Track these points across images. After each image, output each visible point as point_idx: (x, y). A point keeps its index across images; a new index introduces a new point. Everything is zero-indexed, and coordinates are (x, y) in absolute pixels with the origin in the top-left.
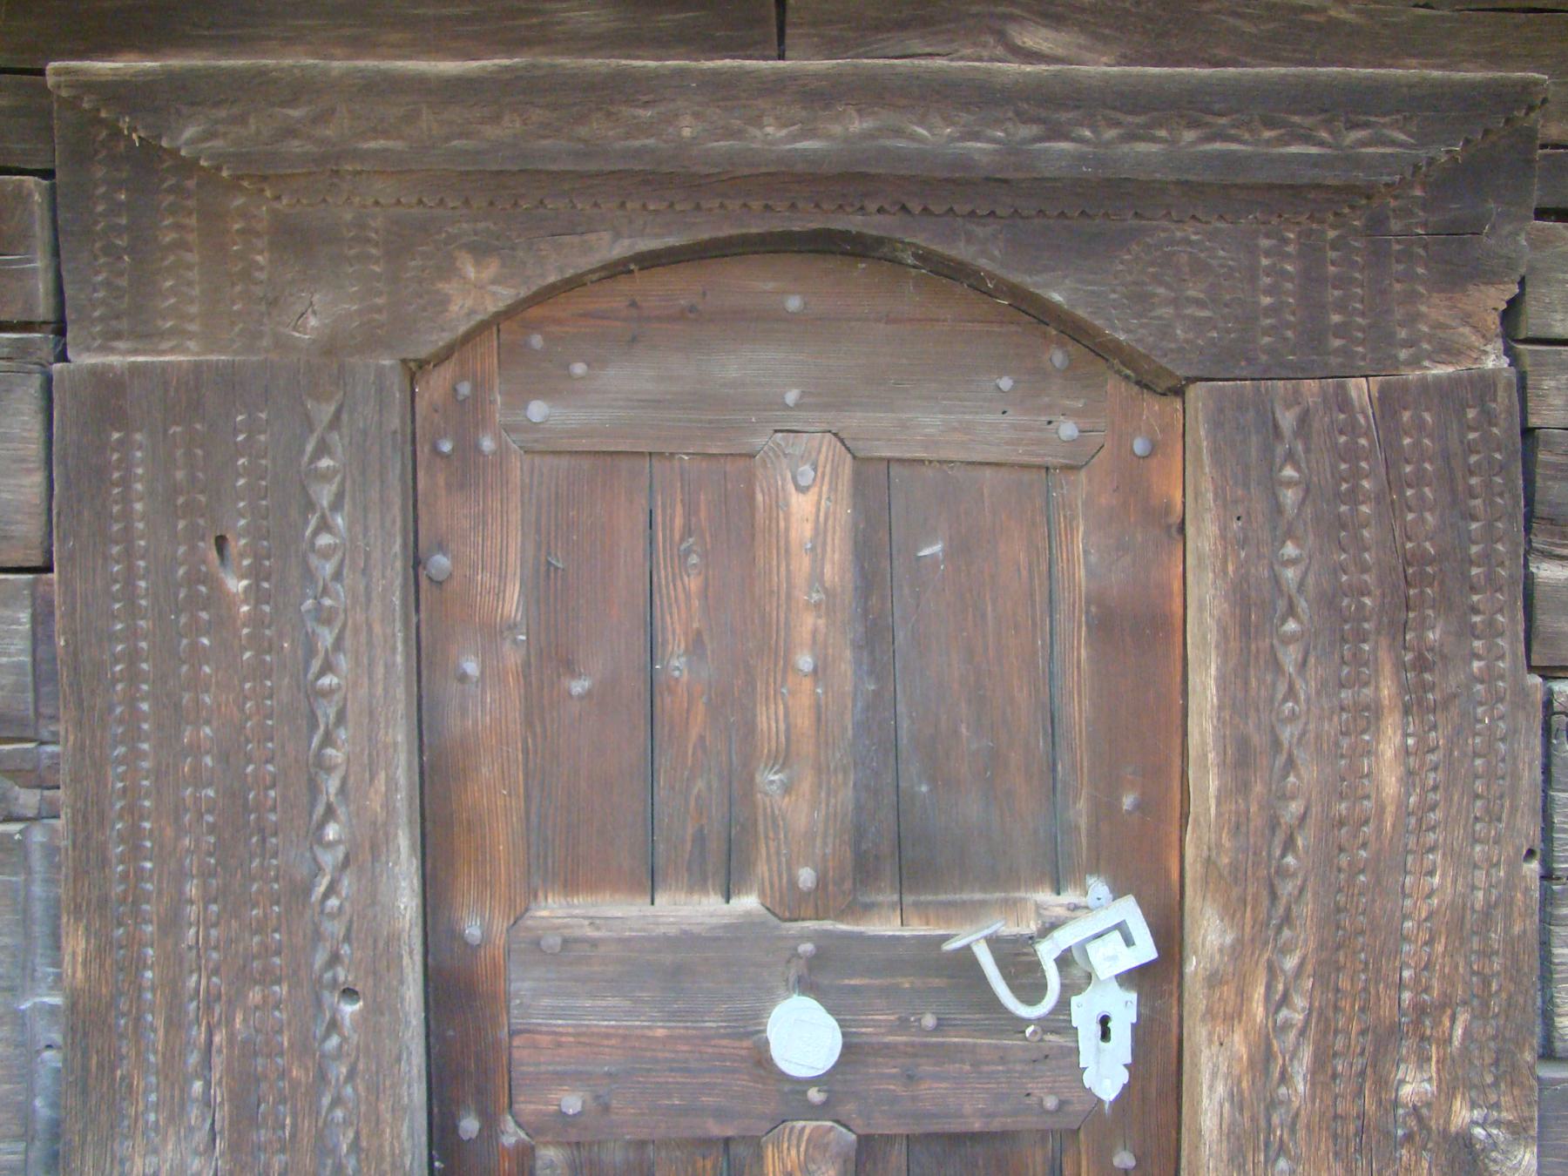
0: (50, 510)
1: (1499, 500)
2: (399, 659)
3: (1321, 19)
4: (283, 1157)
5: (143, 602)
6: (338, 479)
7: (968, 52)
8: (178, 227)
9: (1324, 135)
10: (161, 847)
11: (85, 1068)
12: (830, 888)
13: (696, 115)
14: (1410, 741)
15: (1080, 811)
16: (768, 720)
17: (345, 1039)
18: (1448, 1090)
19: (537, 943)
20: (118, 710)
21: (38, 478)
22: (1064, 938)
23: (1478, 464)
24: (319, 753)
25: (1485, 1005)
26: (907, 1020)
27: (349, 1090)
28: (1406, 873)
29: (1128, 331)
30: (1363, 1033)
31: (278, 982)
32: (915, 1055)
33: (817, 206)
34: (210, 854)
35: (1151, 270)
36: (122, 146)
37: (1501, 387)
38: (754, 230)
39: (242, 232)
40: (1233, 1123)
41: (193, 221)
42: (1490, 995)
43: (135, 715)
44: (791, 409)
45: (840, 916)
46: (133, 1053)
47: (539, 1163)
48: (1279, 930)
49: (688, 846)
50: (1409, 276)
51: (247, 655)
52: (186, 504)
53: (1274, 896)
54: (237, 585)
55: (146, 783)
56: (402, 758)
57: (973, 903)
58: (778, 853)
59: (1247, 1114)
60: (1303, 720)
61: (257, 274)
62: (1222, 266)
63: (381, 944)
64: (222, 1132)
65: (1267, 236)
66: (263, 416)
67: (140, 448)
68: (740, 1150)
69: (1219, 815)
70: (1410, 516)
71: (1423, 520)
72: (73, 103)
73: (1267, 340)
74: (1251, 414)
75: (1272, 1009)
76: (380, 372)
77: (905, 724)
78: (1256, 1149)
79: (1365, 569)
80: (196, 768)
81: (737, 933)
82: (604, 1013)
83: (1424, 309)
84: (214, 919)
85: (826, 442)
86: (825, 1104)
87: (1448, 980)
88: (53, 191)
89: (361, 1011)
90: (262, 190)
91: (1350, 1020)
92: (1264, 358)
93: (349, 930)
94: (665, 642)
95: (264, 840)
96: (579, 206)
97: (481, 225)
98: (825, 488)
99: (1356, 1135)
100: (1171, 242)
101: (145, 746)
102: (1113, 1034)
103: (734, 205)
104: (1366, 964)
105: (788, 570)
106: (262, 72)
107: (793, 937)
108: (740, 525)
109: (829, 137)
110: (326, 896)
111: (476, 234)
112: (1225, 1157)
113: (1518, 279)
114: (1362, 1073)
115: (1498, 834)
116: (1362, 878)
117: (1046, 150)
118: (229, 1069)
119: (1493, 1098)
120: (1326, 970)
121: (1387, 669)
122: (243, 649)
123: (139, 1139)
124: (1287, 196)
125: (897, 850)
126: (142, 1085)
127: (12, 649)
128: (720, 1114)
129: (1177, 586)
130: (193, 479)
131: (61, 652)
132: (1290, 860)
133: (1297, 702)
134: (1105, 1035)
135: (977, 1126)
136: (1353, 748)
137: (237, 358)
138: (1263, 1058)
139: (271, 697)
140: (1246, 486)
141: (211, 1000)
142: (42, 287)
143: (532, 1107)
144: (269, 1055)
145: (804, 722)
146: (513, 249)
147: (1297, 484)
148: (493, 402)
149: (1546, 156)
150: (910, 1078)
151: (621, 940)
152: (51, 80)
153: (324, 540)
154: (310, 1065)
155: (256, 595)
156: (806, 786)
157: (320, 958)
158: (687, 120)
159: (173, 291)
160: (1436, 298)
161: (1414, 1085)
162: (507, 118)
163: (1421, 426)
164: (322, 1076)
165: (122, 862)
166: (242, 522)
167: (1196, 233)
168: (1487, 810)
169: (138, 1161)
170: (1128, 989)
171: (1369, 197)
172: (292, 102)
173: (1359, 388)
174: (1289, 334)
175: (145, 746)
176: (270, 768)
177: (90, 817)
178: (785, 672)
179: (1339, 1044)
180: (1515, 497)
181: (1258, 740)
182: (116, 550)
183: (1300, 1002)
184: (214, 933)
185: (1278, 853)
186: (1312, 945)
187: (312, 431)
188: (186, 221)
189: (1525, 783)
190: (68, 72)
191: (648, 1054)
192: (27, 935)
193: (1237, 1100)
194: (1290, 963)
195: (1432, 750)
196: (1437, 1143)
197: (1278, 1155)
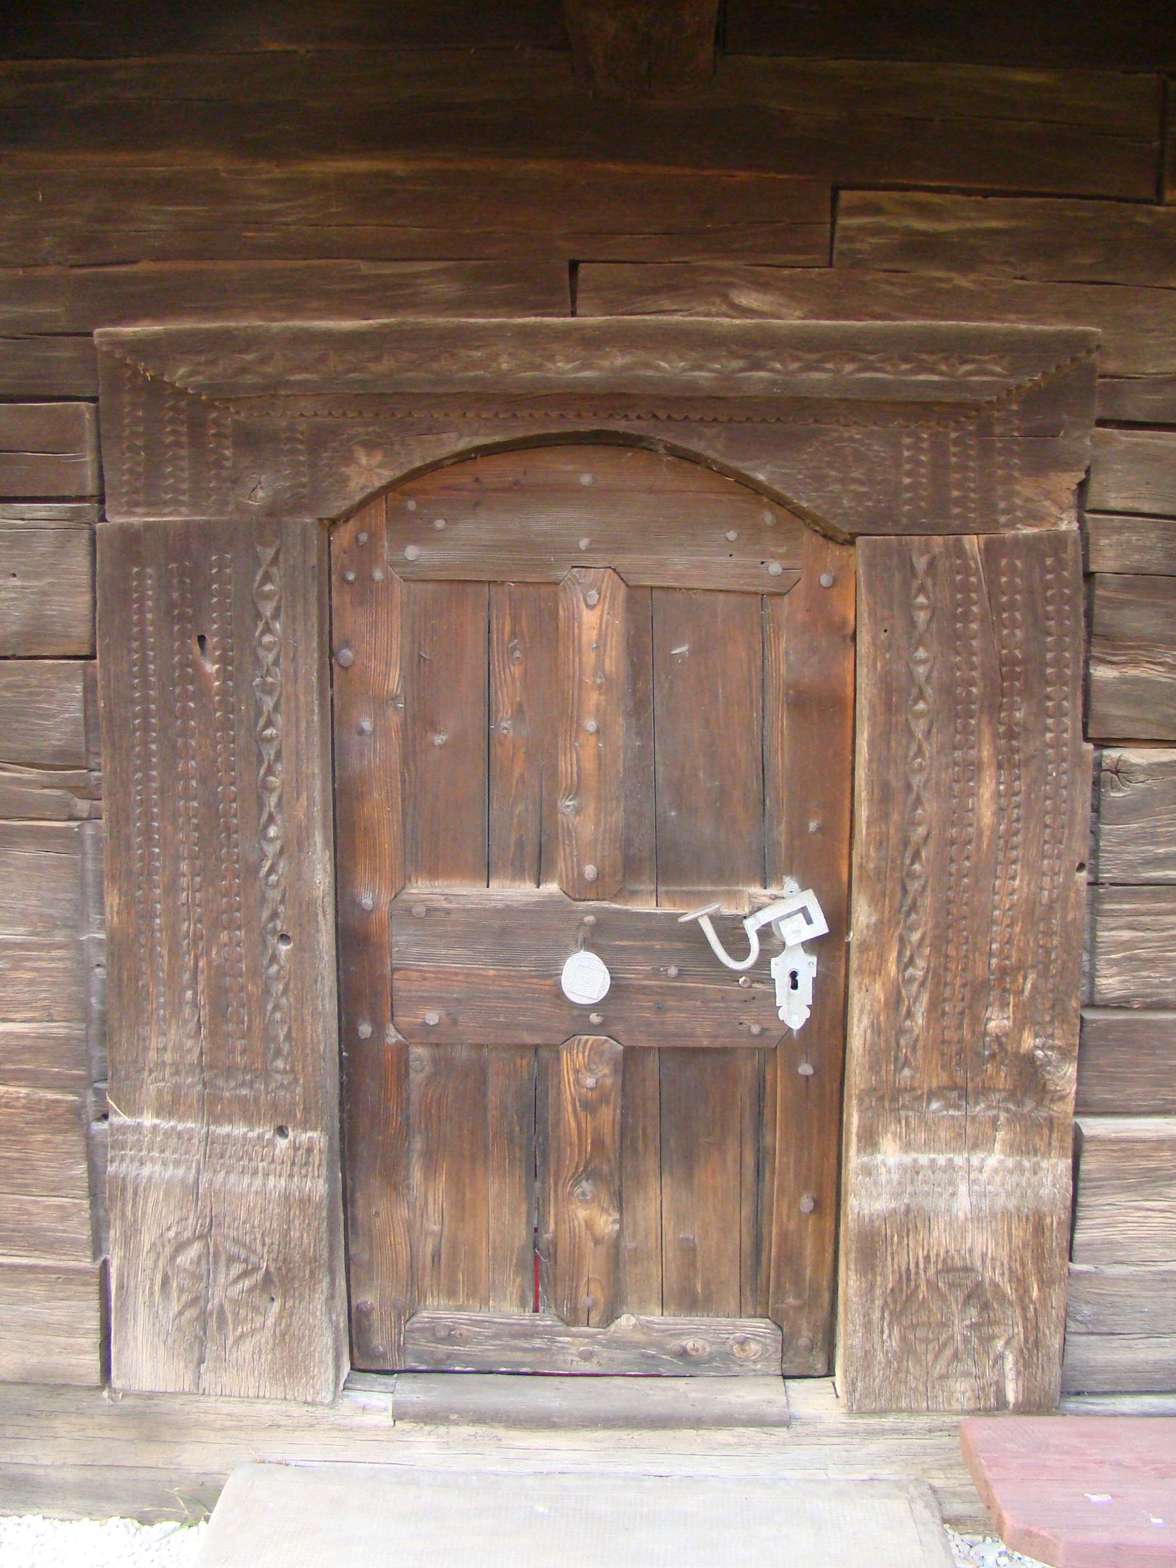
0: (94, 618)
1: (1067, 622)
2: (316, 718)
4: (243, 1042)
5: (153, 679)
6: (276, 598)
7: (702, 309)
8: (174, 432)
9: (944, 368)
10: (165, 839)
11: (120, 979)
12: (607, 879)
13: (510, 355)
14: (1002, 787)
15: (781, 832)
16: (566, 765)
17: (281, 967)
20: (137, 749)
21: (87, 598)
22: (764, 917)
23: (1053, 596)
24: (264, 780)
25: (1047, 968)
26: (658, 970)
27: (284, 1000)
28: (997, 877)
29: (809, 500)
30: (964, 985)
31: (239, 928)
33: (595, 414)
34: (195, 844)
35: (827, 459)
36: (140, 381)
38: (553, 431)
39: (214, 435)
40: (872, 1044)
41: (184, 429)
42: (1051, 962)
43: (148, 754)
44: (582, 552)
45: (614, 897)
46: (149, 971)
47: (412, 1057)
48: (908, 914)
49: (512, 849)
50: (1005, 465)
51: (218, 714)
52: (179, 614)
53: (905, 891)
54: (211, 668)
56: (318, 783)
57: (706, 892)
58: (571, 853)
59: (883, 1038)
60: (927, 771)
62: (876, 457)
65: (908, 436)
66: (228, 556)
67: (150, 577)
68: (543, 1053)
69: (868, 834)
70: (1005, 632)
71: (1013, 635)
72: (109, 355)
73: (907, 508)
74: (895, 559)
75: (902, 967)
77: (661, 769)
78: (888, 1062)
79: (973, 667)
82: (454, 959)
83: (1018, 488)
85: (607, 576)
86: (601, 1024)
88: (97, 411)
89: (292, 950)
90: (228, 408)
91: (955, 977)
92: (904, 520)
93: (284, 896)
94: (497, 711)
95: (229, 836)
96: (435, 416)
97: (371, 429)
99: (957, 1054)
101: (154, 773)
102: (788, 975)
103: (538, 414)
104: (967, 938)
108: (548, 631)
109: (600, 369)
110: (269, 873)
112: (867, 1066)
113: (1085, 468)
114: (962, 1013)
116: (966, 880)
117: (749, 378)
119: (1049, 1031)
121: (987, 736)
122: (216, 710)
124: (921, 409)
125: (654, 856)
128: (531, 1029)
129: (850, 678)
130: (183, 597)
131: (101, 712)
132: (917, 867)
133: (924, 758)
134: (795, 986)
135: (706, 1043)
136: (962, 791)
137: (213, 518)
138: (895, 1001)
139: (233, 742)
140: (891, 609)
141: (197, 938)
142: (90, 472)
144: (233, 976)
145: (589, 765)
146: (392, 444)
147: (927, 607)
148: (383, 546)
149: (1105, 384)
150: (660, 1009)
151: (465, 910)
152: (96, 341)
153: (268, 638)
154: (259, 982)
155: (224, 674)
156: (591, 810)
157: (265, 914)
159: (172, 475)
161: (997, 1022)
162: (386, 358)
163: (1012, 570)
164: (267, 991)
166: (215, 626)
168: (1053, 836)
169: (154, 1039)
170: (812, 954)
171: (977, 410)
172: (246, 351)
173: (971, 542)
174: (923, 504)
175: (154, 773)
176: (233, 788)
177: (120, 819)
178: (577, 731)
179: (947, 992)
180: (1078, 622)
181: (897, 784)
182: (135, 644)
183: (921, 963)
184: (198, 895)
185: (908, 861)
186: (930, 925)
187: (260, 566)
188: (179, 429)
189: (1079, 818)
192: (84, 893)
193: (876, 1028)
194: (915, 937)
195: (1017, 794)
196: (1011, 1061)
197: (903, 1068)
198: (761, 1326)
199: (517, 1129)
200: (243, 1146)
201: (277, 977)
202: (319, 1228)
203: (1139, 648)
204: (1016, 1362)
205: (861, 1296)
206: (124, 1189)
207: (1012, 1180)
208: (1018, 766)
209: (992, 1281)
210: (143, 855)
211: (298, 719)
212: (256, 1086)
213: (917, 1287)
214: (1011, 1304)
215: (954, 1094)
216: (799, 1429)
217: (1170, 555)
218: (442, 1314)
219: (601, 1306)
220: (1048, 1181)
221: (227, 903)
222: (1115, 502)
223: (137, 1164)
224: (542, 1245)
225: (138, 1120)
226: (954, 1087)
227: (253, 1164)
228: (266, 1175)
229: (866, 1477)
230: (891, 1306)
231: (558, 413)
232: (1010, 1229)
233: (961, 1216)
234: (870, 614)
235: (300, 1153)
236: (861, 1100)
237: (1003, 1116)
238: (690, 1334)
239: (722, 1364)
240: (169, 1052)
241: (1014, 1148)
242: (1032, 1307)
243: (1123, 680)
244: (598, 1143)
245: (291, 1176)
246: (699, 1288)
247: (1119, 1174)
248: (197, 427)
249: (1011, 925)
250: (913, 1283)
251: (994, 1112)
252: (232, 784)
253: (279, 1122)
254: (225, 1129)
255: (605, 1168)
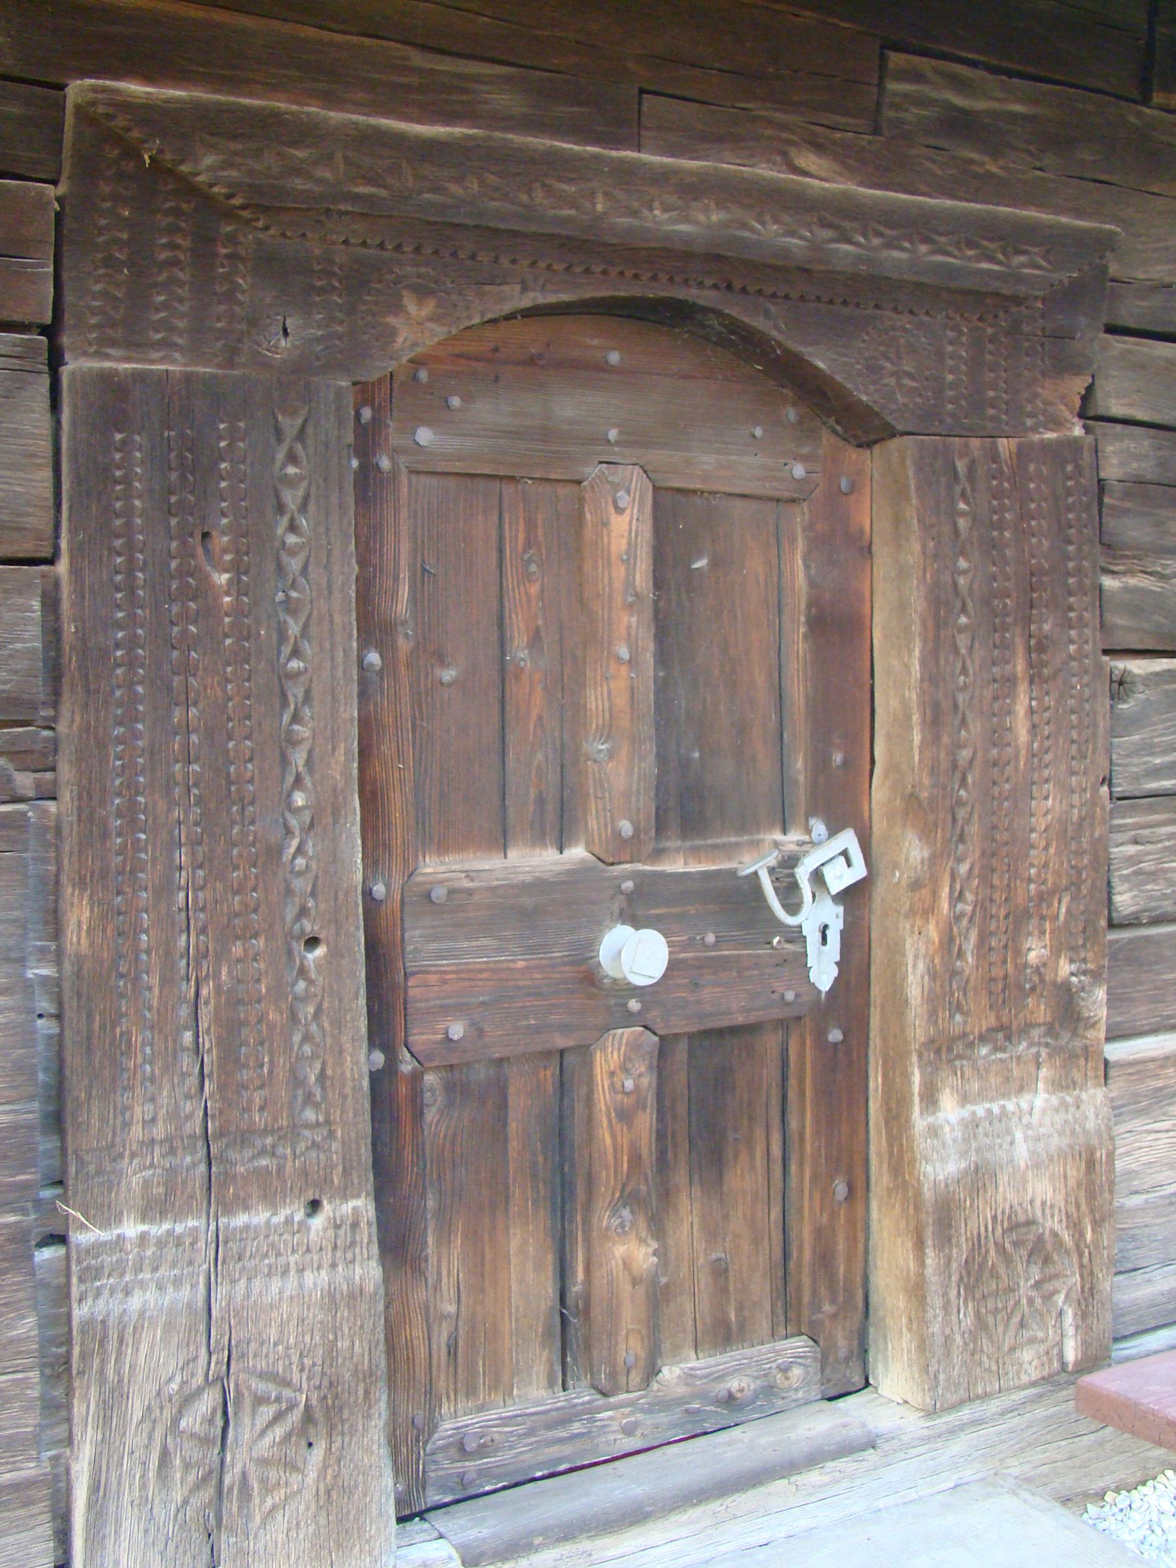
3: (980, 170)
5: (141, 592)
6: (305, 484)
14: (1034, 703)
18: (1056, 952)
19: (428, 896)
20: (118, 693)
21: (48, 473)
23: (1073, 503)
29: (868, 394)
30: (1007, 916)
31: (255, 936)
32: (700, 967)
34: (196, 824)
37: (1086, 448)
38: (622, 294)
39: (228, 257)
40: (931, 990)
49: (531, 809)
52: (178, 502)
53: (954, 820)
55: (141, 760)
61: (239, 296)
63: (341, 896)
64: (211, 1075)
65: (952, 329)
67: (140, 450)
68: (569, 1059)
76: (339, 391)
79: (1007, 579)
80: (186, 746)
81: (575, 877)
82: (479, 953)
83: (1040, 390)
84: (201, 883)
86: (640, 1013)
87: (1058, 873)
89: (326, 956)
92: (949, 420)
93: (314, 886)
95: (243, 809)
97: (423, 270)
98: (635, 511)
100: (894, 328)
105: (610, 578)
106: (276, 114)
107: (617, 878)
108: (571, 540)
109: (697, 223)
111: (418, 277)
114: (1006, 947)
115: (1086, 768)
117: (837, 250)
118: (217, 1018)
119: (1082, 954)
120: (986, 873)
123: (138, 1090)
126: (140, 1039)
127: (27, 635)
135: (740, 1019)
139: (249, 680)
143: (423, 1037)
145: (622, 701)
154: (284, 1006)
155: (237, 587)
156: (624, 751)
157: (290, 913)
158: (600, 198)
159: (166, 306)
160: (1048, 383)
161: (1036, 951)
164: (294, 1017)
165: (119, 835)
167: (909, 323)
168: (1079, 751)
169: (138, 1110)
172: (295, 144)
174: (964, 403)
179: (993, 926)
181: (946, 704)
182: (118, 543)
184: (201, 895)
188: (180, 241)
190: (104, 90)
191: (511, 983)
194: (963, 869)
198: (799, 1345)
199: (541, 1159)
200: (267, 1237)
201: (305, 999)
202: (375, 1328)
203: (1134, 558)
204: (1075, 1315)
205: (940, 1275)
206: (105, 1336)
207: (1059, 1119)
208: (1046, 682)
209: (1051, 1230)
210: (124, 845)
211: (333, 648)
212: (280, 1151)
213: (987, 1251)
214: (1067, 1252)
215: (1000, 1036)
216: (886, 1447)
217: (1162, 464)
218: (466, 1420)
219: (642, 1363)
220: (1091, 1115)
221: (241, 902)
222: (1117, 409)
223: (120, 1296)
224: (570, 1301)
225: (119, 1231)
226: (1001, 1028)
227: (282, 1260)
228: (301, 1271)
229: (952, 1485)
230: (966, 1280)
231: (633, 272)
232: (1065, 1170)
233: (1022, 1164)
234: (919, 521)
235: (342, 1232)
236: (920, 1055)
237: (1044, 1052)
238: (733, 1373)
239: (767, 1400)
240: (160, 1123)
241: (1061, 1084)
242: (1086, 1251)
243: (1127, 589)
244: (636, 1160)
245: (334, 1266)
246: (733, 1316)
247: (1136, 1097)
248: (204, 242)
249: (1046, 848)
250: (983, 1250)
251: (1034, 1050)
252: (247, 738)
253: (310, 1196)
254: (241, 1219)
255: (643, 1188)
